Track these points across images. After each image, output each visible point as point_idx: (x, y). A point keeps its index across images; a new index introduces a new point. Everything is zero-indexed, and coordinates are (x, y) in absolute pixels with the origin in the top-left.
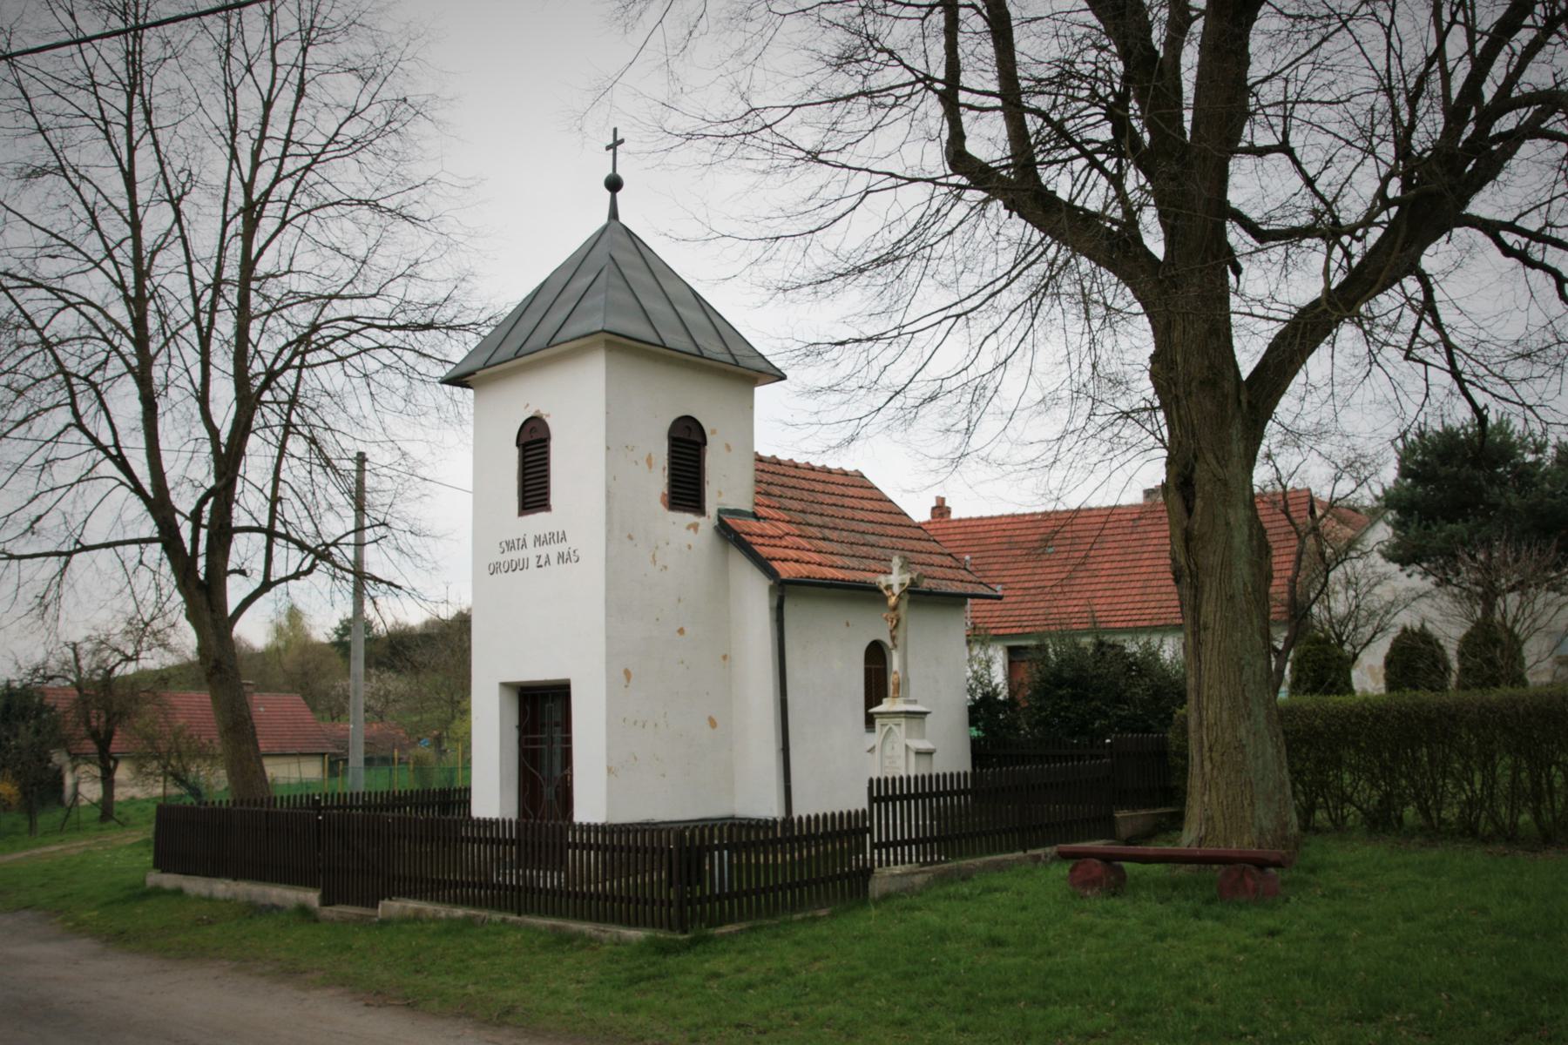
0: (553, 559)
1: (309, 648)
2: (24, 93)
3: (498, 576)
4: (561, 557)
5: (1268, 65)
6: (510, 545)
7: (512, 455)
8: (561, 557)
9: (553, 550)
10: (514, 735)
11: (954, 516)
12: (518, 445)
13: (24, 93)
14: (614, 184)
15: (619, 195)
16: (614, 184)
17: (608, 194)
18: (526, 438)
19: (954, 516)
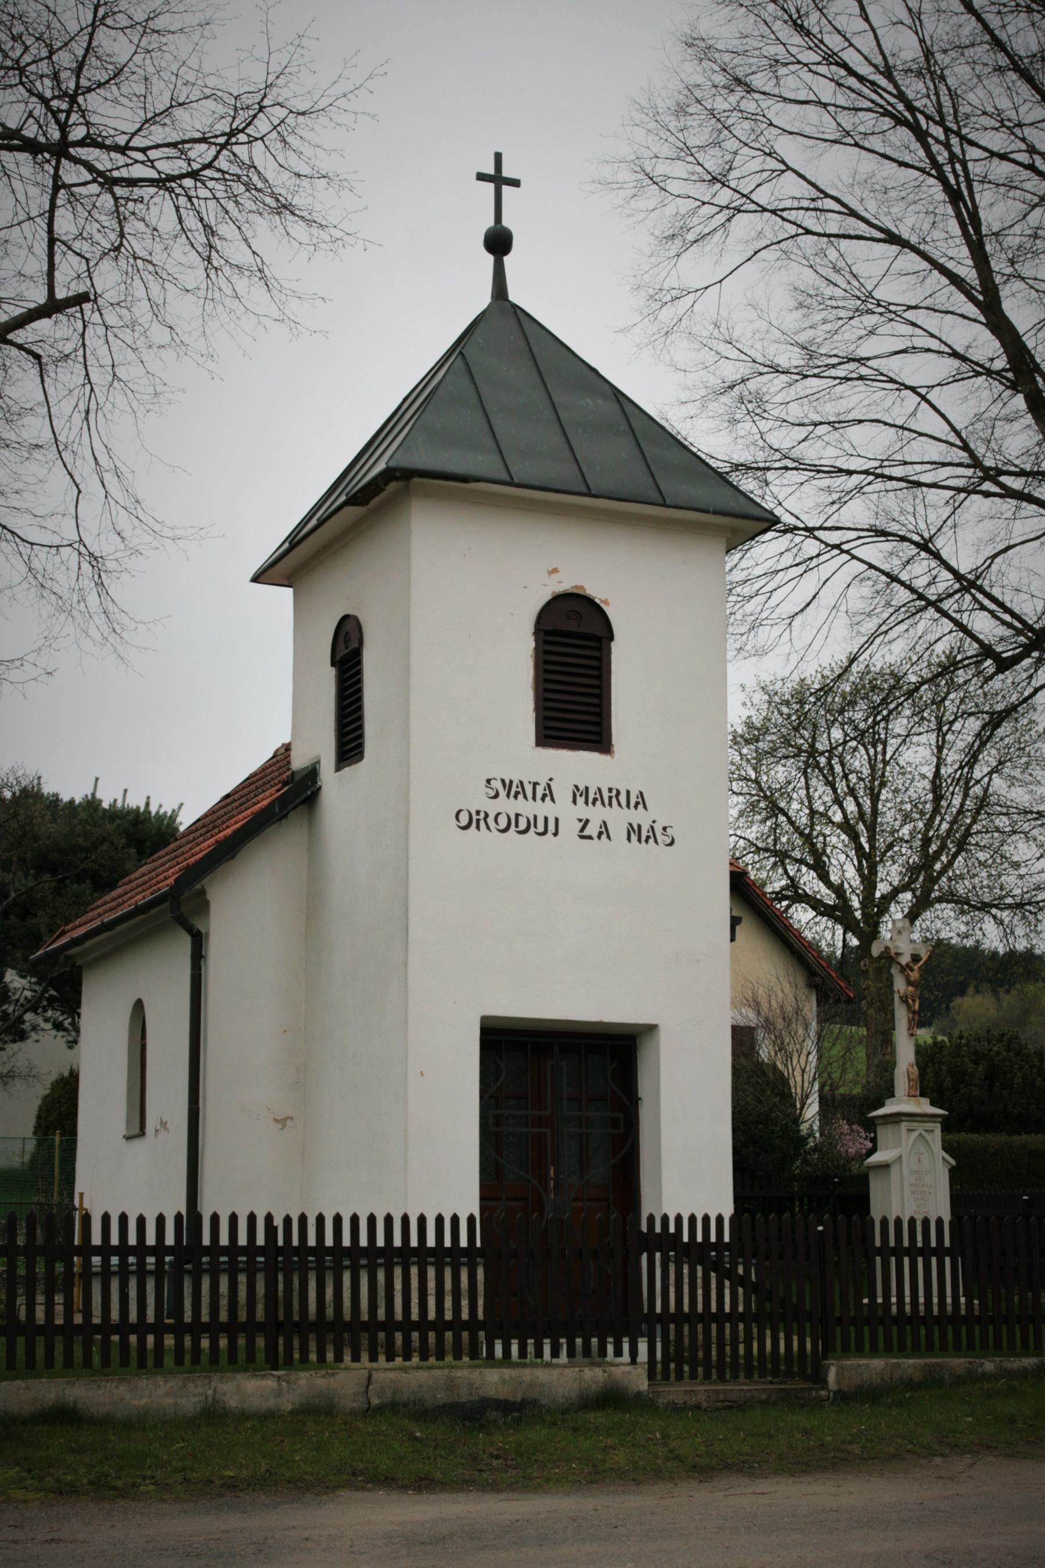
0: (618, 831)
1: (1033, 954)
2: (85, 361)
3: (94, 780)
4: (634, 832)
5: (78, 365)
6: (513, 789)
7: (329, 675)
8: (634, 832)
9: (618, 818)
10: (644, 1090)
11: (185, 821)
12: (333, 664)
13: (85, 361)
14: (499, 243)
15: (507, 259)
16: (499, 243)
17: (490, 258)
18: (342, 652)
19: (185, 821)
